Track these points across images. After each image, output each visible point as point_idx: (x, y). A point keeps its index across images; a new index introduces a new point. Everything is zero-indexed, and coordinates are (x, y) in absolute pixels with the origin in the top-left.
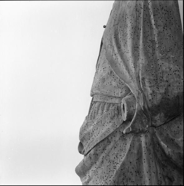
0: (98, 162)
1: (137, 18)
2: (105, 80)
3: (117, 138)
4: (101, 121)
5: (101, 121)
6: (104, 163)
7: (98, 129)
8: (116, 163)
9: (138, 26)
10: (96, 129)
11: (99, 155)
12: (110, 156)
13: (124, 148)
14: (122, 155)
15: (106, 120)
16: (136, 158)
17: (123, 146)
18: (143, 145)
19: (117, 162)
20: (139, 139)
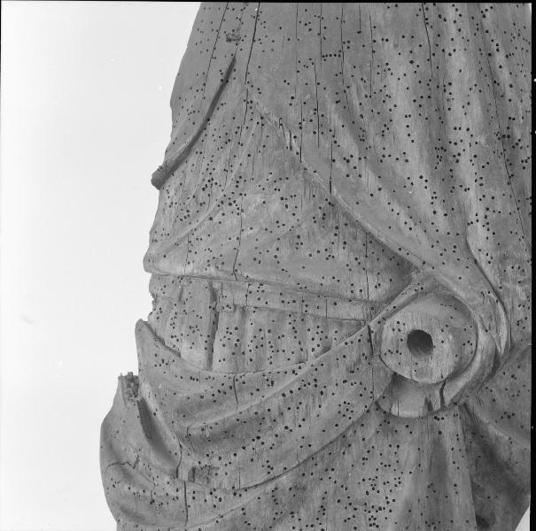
0: (303, 511)
1: (432, 52)
2: (301, 240)
3: (370, 430)
4: (316, 380)
5: (316, 380)
6: (329, 511)
7: (303, 407)
8: (373, 507)
9: (435, 76)
10: (293, 406)
11: (309, 487)
12: (349, 486)
13: (395, 460)
14: (391, 479)
15: (333, 375)
16: (427, 483)
17: (389, 453)
18: (449, 443)
19: (377, 506)
20: (432, 426)
